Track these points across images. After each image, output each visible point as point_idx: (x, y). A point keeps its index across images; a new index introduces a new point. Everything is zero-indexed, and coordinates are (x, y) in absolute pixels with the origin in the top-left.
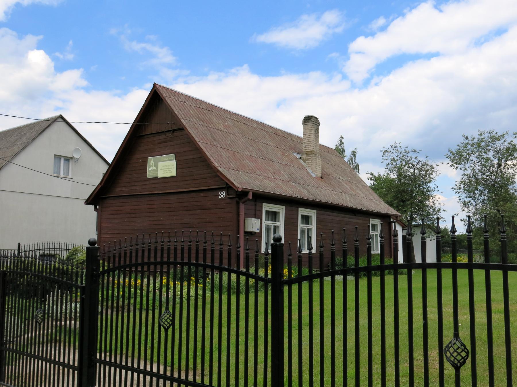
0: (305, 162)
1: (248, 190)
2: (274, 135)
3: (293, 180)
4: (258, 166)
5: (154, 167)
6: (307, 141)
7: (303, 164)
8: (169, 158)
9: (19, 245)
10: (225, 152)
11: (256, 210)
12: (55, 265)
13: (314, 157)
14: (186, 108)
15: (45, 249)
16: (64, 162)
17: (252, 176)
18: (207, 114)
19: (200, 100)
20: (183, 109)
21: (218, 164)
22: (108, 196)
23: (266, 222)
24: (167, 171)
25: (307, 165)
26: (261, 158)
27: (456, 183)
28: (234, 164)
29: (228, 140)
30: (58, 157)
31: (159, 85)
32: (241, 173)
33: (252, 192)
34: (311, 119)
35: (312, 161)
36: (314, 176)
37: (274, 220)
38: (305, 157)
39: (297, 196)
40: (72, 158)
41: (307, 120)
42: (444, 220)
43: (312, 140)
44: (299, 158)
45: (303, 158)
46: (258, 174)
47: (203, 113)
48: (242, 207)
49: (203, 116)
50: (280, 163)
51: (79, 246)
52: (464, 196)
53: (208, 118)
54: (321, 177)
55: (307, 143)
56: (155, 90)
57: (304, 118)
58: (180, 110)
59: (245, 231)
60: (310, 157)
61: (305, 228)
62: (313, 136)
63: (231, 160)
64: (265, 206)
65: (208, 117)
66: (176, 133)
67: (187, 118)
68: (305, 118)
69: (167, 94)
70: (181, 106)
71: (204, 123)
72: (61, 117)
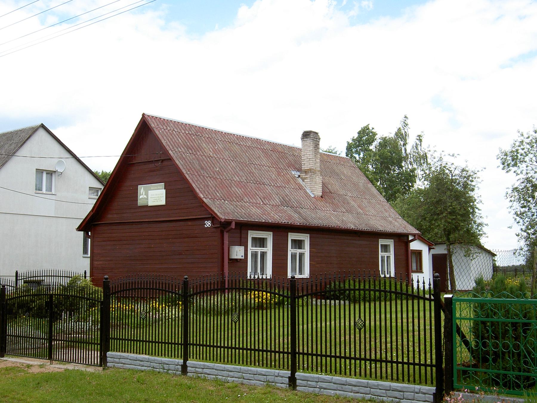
0: (303, 181)
1: (231, 220)
2: (271, 152)
3: (285, 203)
4: (246, 192)
5: (145, 195)
6: (306, 158)
7: (302, 184)
8: (159, 187)
9: (17, 273)
10: (212, 181)
11: (241, 237)
12: (90, 292)
13: (313, 176)
14: (174, 137)
15: (42, 276)
16: (46, 177)
17: (238, 204)
18: (196, 140)
19: (189, 125)
20: (171, 138)
21: (203, 195)
22: (99, 223)
23: (252, 248)
24: (156, 199)
25: (305, 184)
26: (252, 182)
27: (508, 190)
28: (220, 192)
29: (216, 166)
30: (39, 171)
31: (148, 115)
32: (226, 202)
33: (235, 222)
34: (309, 134)
35: (311, 180)
36: (313, 196)
37: (262, 246)
38: (303, 175)
39: (284, 222)
40: (55, 172)
41: (306, 135)
42: (486, 235)
43: (311, 157)
44: (297, 176)
45: (301, 176)
46: (245, 201)
47: (192, 139)
48: (226, 236)
49: (191, 144)
50: (273, 185)
51: (79, 274)
52: (517, 206)
53: (196, 144)
54: (322, 197)
55: (305, 160)
56: (144, 120)
57: (303, 133)
58: (168, 140)
59: (230, 258)
60: (309, 176)
61: (296, 253)
62: (312, 153)
63: (218, 189)
64: (250, 233)
65: (197, 142)
66: (165, 163)
67: (175, 148)
68: (304, 134)
69: (156, 124)
70: (170, 135)
71: (192, 151)
72: (43, 126)
